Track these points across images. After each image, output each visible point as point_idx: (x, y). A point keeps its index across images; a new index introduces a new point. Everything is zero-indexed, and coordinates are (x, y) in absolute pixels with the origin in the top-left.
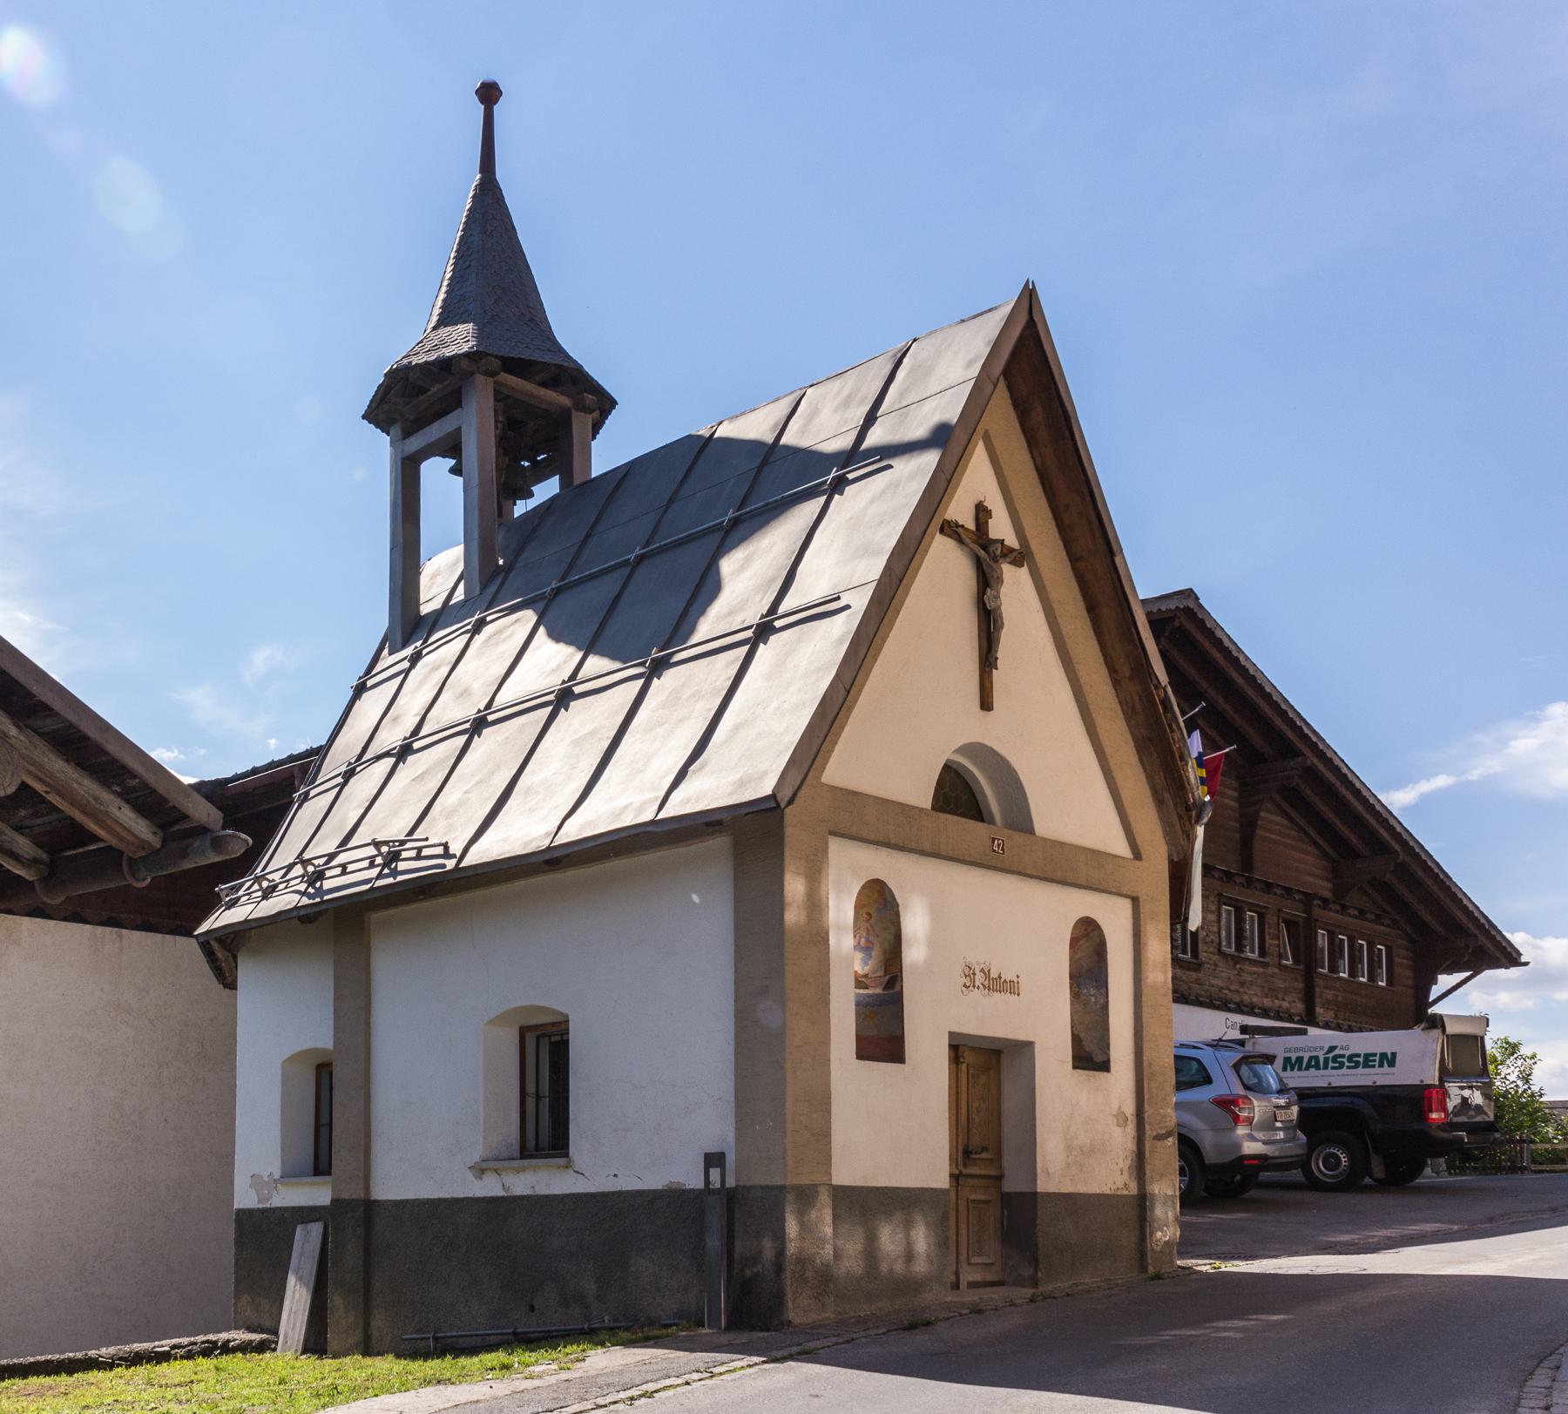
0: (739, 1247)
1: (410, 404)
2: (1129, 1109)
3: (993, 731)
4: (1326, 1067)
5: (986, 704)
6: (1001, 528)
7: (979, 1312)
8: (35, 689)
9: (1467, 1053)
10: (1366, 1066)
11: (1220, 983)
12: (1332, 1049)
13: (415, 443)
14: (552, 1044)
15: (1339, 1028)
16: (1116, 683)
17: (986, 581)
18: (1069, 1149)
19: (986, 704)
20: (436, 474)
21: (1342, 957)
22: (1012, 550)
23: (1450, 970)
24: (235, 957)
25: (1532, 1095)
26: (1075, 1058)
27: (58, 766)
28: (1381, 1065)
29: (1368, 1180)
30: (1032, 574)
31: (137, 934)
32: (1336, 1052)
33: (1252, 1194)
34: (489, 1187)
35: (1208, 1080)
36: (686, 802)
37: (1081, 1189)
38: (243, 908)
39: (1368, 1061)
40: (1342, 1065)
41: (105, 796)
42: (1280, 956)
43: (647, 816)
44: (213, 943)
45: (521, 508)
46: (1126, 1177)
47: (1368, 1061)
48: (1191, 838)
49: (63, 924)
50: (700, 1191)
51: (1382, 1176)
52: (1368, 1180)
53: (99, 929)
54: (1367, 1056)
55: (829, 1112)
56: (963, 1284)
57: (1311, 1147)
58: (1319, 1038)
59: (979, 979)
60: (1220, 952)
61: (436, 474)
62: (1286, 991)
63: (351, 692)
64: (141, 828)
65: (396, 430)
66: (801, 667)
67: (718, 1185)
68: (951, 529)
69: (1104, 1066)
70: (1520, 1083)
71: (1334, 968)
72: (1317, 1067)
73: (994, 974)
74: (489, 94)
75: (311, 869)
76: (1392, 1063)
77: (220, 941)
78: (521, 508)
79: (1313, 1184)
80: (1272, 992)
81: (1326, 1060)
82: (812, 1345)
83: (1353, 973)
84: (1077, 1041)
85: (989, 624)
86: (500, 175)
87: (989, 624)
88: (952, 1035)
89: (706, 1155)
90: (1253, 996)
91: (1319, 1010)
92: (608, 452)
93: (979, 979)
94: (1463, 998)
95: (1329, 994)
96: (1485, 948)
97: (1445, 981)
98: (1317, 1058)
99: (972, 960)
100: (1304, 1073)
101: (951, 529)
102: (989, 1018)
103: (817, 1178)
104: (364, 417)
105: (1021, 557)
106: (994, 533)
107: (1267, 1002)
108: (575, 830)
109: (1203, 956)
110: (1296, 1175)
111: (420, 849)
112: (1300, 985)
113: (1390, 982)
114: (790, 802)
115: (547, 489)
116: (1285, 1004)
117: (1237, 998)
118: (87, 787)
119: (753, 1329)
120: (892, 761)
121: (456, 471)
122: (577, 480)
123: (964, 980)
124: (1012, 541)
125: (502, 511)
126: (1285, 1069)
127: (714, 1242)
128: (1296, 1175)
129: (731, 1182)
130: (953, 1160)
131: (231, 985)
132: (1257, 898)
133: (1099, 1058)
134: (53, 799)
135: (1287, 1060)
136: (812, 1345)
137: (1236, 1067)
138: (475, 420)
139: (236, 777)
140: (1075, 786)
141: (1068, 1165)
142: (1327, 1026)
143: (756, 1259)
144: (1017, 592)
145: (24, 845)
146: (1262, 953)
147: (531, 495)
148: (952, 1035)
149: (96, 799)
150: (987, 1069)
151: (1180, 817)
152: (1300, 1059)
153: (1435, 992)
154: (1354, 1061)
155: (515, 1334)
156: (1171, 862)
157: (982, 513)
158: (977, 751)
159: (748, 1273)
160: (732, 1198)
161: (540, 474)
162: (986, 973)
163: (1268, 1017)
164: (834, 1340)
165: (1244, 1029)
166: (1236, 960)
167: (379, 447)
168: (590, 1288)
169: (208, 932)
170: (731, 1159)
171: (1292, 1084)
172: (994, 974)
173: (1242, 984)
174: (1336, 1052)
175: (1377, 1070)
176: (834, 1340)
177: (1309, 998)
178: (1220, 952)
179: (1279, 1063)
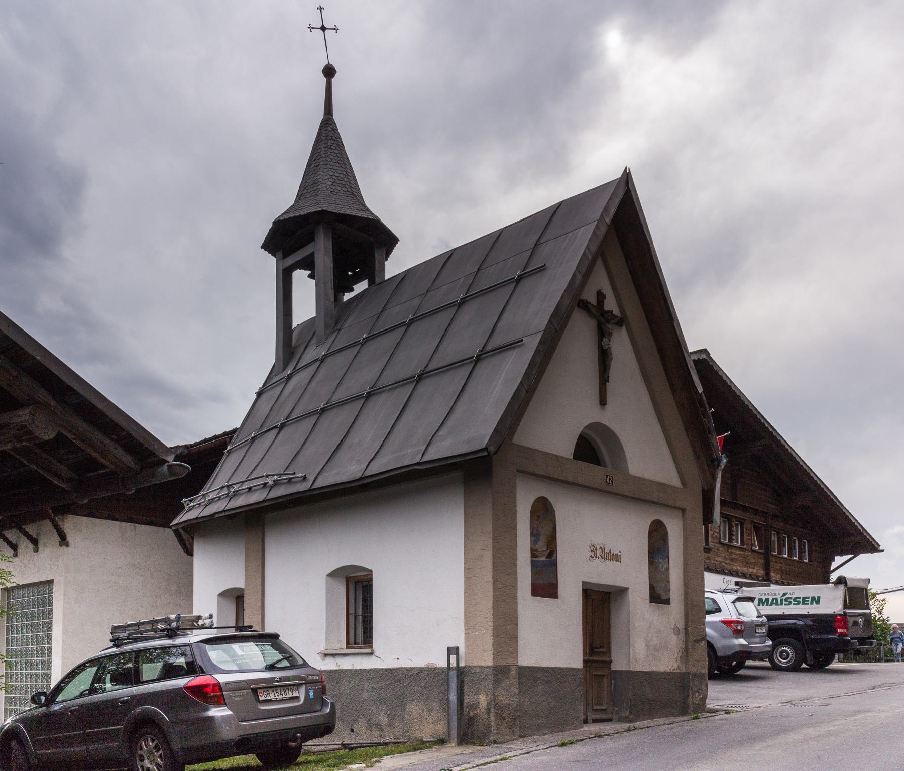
0: (467, 700)
1: (288, 239)
2: (681, 625)
3: (608, 418)
4: (781, 604)
5: (603, 402)
6: (610, 304)
7: (600, 736)
8: (64, 378)
9: (857, 595)
10: (803, 603)
11: (721, 560)
12: (785, 594)
13: (290, 261)
14: (363, 587)
15: (783, 584)
16: (674, 391)
17: (602, 333)
18: (648, 646)
19: (603, 402)
20: (300, 276)
21: (784, 546)
22: (616, 317)
23: (841, 554)
24: (193, 539)
25: (883, 620)
26: (651, 597)
27: (83, 426)
28: (812, 603)
29: (804, 665)
30: (628, 331)
31: (143, 527)
32: (787, 596)
33: (742, 672)
34: (330, 665)
35: (718, 610)
36: (437, 452)
37: (654, 669)
38: (193, 510)
39: (804, 601)
40: (790, 603)
41: (107, 441)
42: (752, 545)
43: (417, 459)
44: (182, 532)
45: (347, 297)
46: (679, 663)
47: (804, 601)
48: (714, 478)
49: (104, 521)
50: (445, 668)
51: (812, 663)
52: (804, 665)
53: (124, 524)
54: (804, 598)
55: (517, 625)
56: (589, 719)
57: (775, 647)
58: (775, 590)
59: (599, 552)
60: (720, 543)
61: (300, 276)
62: (755, 564)
63: (255, 396)
64: (128, 460)
65: (280, 254)
66: (501, 381)
67: (455, 665)
68: (584, 305)
69: (667, 602)
70: (877, 614)
71: (780, 552)
72: (777, 604)
73: (607, 550)
74: (321, 9)
75: (232, 490)
76: (818, 602)
77: (183, 529)
78: (347, 297)
79: (776, 667)
80: (747, 564)
81: (782, 600)
82: (508, 755)
83: (790, 555)
84: (652, 588)
85: (604, 358)
86: (337, 116)
87: (604, 358)
88: (584, 583)
89: (448, 648)
90: (737, 567)
91: (772, 574)
92: (395, 265)
93: (599, 552)
94: (853, 568)
95: (778, 566)
96: (861, 543)
97: (839, 560)
98: (776, 599)
99: (595, 542)
100: (769, 607)
101: (584, 305)
102: (605, 575)
103: (510, 661)
104: (262, 247)
105: (621, 322)
106: (607, 307)
107: (745, 569)
108: (375, 469)
109: (711, 545)
110: (767, 663)
111: (290, 479)
112: (763, 561)
113: (810, 560)
114: (496, 453)
115: (361, 287)
116: (755, 571)
117: (729, 568)
118: (96, 436)
119: (474, 744)
120: (554, 432)
121: (311, 276)
122: (378, 280)
123: (590, 553)
124: (616, 312)
125: (337, 299)
126: (759, 605)
127: (453, 697)
128: (767, 663)
129: (462, 664)
130: (584, 654)
131: (190, 553)
132: (739, 514)
133: (664, 597)
134: (78, 443)
135: (760, 600)
136: (508, 755)
137: (733, 602)
138: (322, 249)
139: (196, 444)
140: (648, 454)
141: (648, 656)
142: (777, 583)
143: (475, 706)
144: (621, 344)
145: (64, 470)
146: (743, 543)
147: (352, 290)
148: (584, 583)
149: (102, 442)
150: (600, 603)
151: (708, 465)
152: (767, 600)
153: (834, 565)
154: (797, 601)
155: (342, 744)
156: (703, 490)
157: (601, 296)
158: (596, 427)
159: (472, 714)
160: (461, 672)
161: (357, 279)
162: (603, 550)
163: (746, 578)
164: (521, 752)
165: (737, 584)
166: (729, 547)
167: (270, 263)
168: (384, 720)
169: (177, 524)
170: (462, 651)
171: (763, 613)
172: (607, 550)
173: (732, 560)
174: (787, 596)
175: (809, 606)
176: (521, 752)
177: (767, 567)
178: (720, 543)
179: (756, 601)
